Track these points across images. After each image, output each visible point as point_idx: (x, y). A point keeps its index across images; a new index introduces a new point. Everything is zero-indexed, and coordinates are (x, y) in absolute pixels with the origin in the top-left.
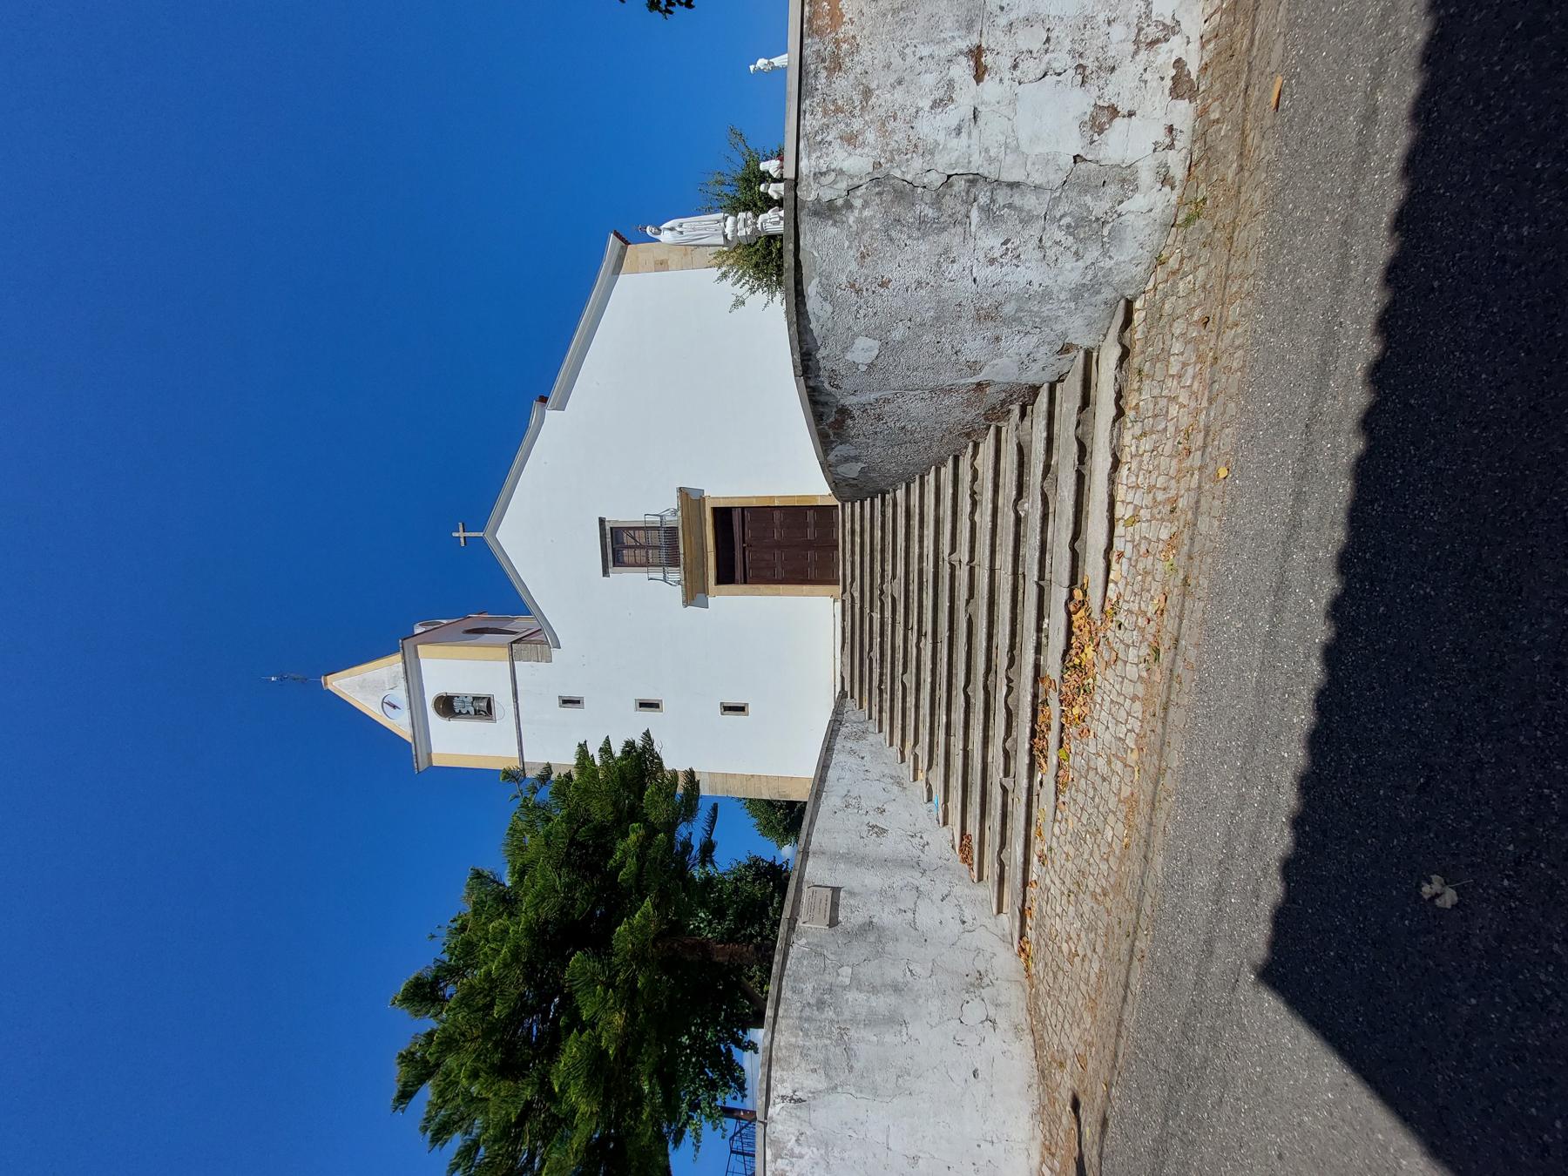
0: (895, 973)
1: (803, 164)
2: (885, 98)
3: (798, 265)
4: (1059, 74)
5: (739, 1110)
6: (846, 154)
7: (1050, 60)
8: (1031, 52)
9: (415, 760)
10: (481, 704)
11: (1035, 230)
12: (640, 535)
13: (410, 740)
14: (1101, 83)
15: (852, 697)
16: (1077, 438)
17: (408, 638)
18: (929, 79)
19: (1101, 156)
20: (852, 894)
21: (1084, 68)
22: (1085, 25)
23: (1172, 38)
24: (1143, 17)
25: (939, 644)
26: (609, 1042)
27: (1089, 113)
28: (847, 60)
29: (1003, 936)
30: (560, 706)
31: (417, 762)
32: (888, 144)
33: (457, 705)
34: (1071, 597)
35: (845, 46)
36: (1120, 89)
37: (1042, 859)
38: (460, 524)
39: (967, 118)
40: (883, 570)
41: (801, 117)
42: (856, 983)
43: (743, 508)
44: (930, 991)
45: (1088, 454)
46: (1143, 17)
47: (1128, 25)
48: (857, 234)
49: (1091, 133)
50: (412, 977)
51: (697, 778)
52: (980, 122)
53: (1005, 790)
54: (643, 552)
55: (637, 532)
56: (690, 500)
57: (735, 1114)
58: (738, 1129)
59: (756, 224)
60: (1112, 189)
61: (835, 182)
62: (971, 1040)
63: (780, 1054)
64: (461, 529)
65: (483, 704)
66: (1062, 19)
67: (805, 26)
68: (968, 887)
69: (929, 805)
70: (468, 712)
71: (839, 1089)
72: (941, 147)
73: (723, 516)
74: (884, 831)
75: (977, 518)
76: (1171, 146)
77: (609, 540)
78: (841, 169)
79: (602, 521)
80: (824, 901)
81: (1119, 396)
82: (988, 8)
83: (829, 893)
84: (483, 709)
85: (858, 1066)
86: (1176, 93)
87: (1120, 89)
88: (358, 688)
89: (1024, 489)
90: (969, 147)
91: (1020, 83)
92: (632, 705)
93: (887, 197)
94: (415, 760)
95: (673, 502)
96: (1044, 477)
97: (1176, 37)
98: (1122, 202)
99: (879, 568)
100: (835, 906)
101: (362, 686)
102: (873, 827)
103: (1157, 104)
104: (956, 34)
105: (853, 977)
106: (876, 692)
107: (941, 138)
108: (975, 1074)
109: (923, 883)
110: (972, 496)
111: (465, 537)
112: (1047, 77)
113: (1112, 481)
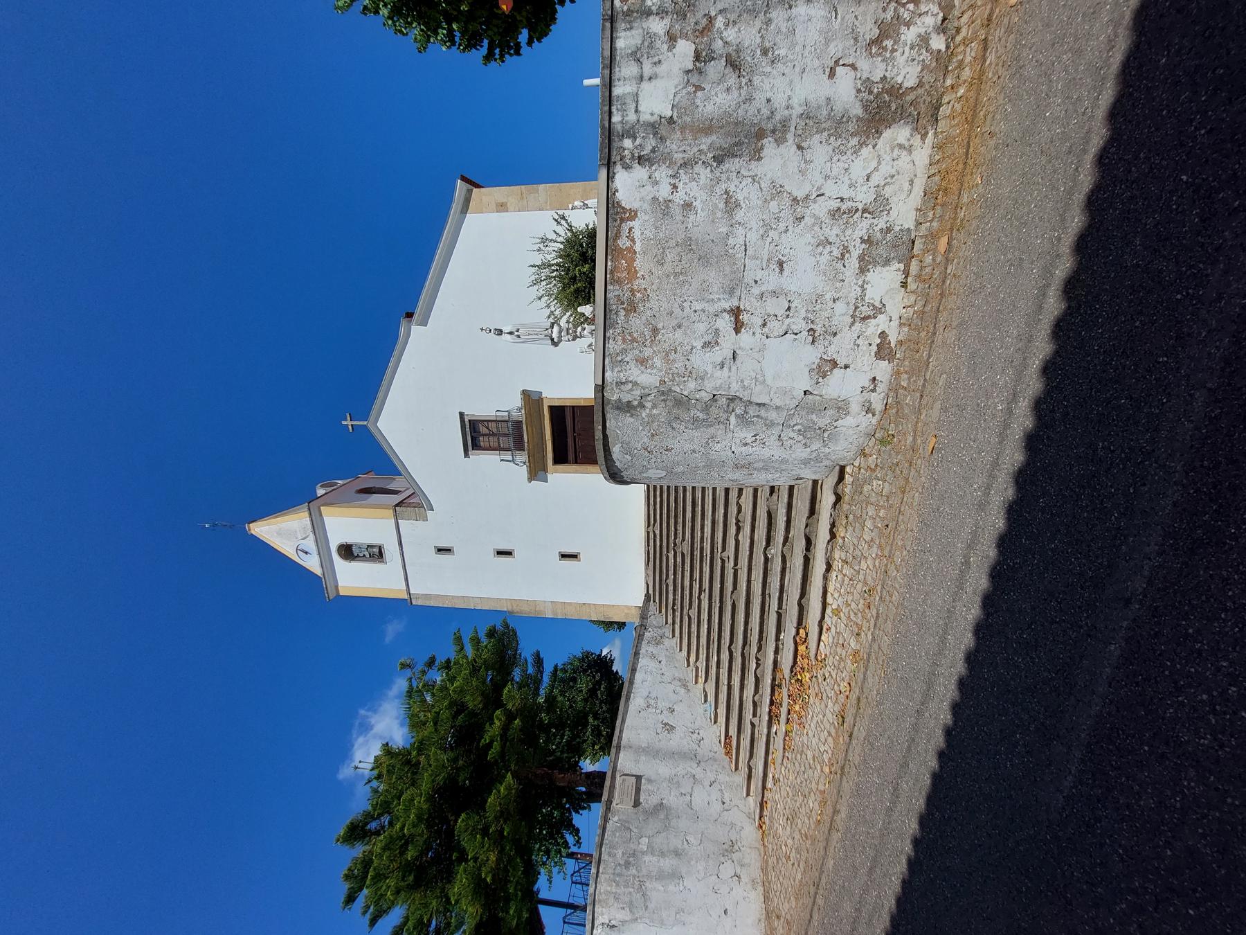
0: (676, 842)
1: (608, 374)
2: (669, 337)
3: (605, 437)
4: (796, 334)
5: (577, 853)
6: (640, 372)
7: (790, 323)
8: (776, 316)
9: (326, 592)
10: (374, 550)
11: (776, 431)
12: (493, 426)
13: (318, 572)
14: (826, 343)
15: (654, 601)
16: (805, 535)
17: (313, 501)
18: (701, 327)
19: (824, 393)
20: (650, 781)
21: (814, 331)
22: (817, 300)
23: (879, 316)
24: (859, 299)
25: (713, 604)
26: (486, 874)
27: (816, 363)
28: (640, 305)
29: (749, 813)
30: (436, 553)
31: (328, 593)
32: (670, 369)
33: (355, 551)
34: (798, 633)
35: (638, 295)
36: (839, 348)
37: (775, 781)
38: (348, 416)
39: (728, 357)
40: (676, 529)
41: (606, 342)
42: (651, 850)
43: (573, 407)
44: (699, 855)
45: (813, 545)
46: (859, 299)
47: (848, 304)
48: (648, 423)
49: (817, 377)
50: (348, 822)
51: (541, 656)
52: (737, 362)
53: (753, 725)
54: (495, 439)
55: (489, 423)
56: (531, 400)
57: (575, 856)
58: (577, 869)
59: (576, 332)
60: (830, 412)
61: (631, 390)
62: (724, 889)
63: (600, 898)
64: (349, 418)
65: (376, 550)
66: (800, 295)
67: (608, 276)
68: (728, 775)
69: (705, 706)
70: (364, 555)
71: (639, 921)
72: (709, 375)
73: (558, 413)
74: (673, 728)
75: (740, 537)
76: (874, 390)
77: (468, 430)
78: (636, 382)
79: (462, 415)
80: (630, 787)
81: (833, 525)
82: (746, 281)
83: (633, 780)
84: (376, 554)
85: (651, 906)
86: (879, 355)
87: (839, 348)
88: (275, 534)
89: (772, 540)
90: (729, 377)
91: (767, 338)
92: (492, 553)
93: (670, 404)
94: (326, 592)
95: (518, 401)
96: (784, 545)
97: (882, 316)
98: (838, 420)
99: (673, 528)
100: (638, 790)
101: (279, 533)
102: (666, 724)
103: (865, 362)
104: (722, 296)
105: (650, 846)
106: (670, 611)
107: (709, 369)
108: (725, 912)
109: (697, 771)
110: (737, 524)
111: (352, 425)
112: (787, 335)
113: (825, 578)
